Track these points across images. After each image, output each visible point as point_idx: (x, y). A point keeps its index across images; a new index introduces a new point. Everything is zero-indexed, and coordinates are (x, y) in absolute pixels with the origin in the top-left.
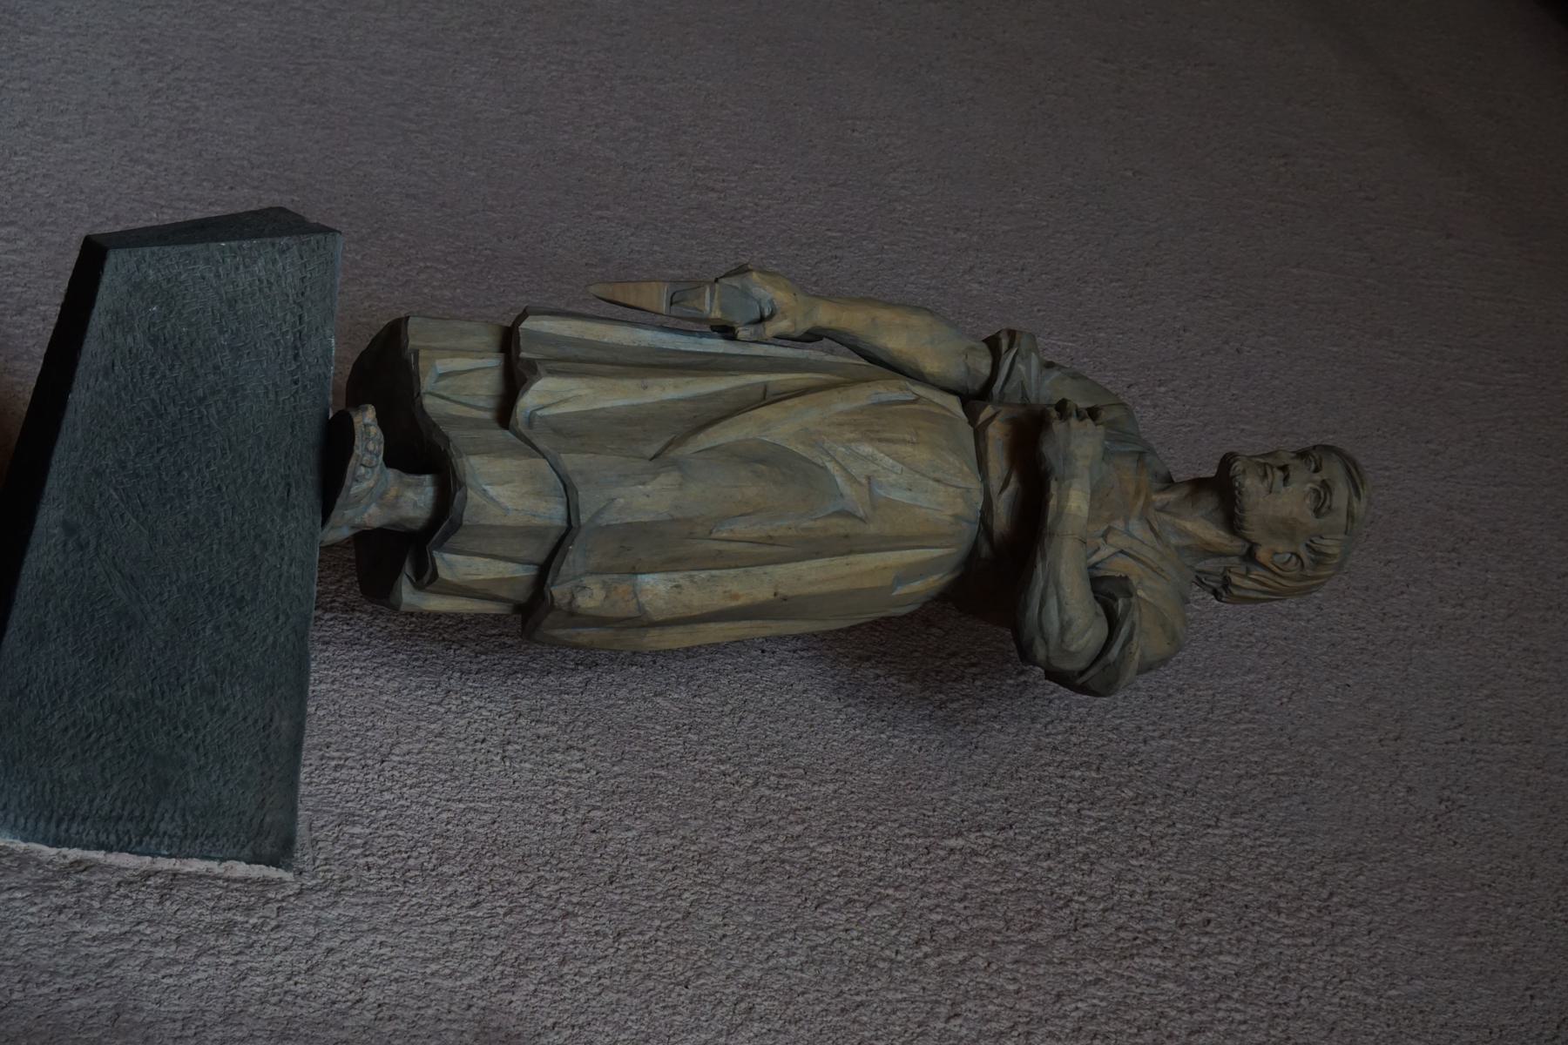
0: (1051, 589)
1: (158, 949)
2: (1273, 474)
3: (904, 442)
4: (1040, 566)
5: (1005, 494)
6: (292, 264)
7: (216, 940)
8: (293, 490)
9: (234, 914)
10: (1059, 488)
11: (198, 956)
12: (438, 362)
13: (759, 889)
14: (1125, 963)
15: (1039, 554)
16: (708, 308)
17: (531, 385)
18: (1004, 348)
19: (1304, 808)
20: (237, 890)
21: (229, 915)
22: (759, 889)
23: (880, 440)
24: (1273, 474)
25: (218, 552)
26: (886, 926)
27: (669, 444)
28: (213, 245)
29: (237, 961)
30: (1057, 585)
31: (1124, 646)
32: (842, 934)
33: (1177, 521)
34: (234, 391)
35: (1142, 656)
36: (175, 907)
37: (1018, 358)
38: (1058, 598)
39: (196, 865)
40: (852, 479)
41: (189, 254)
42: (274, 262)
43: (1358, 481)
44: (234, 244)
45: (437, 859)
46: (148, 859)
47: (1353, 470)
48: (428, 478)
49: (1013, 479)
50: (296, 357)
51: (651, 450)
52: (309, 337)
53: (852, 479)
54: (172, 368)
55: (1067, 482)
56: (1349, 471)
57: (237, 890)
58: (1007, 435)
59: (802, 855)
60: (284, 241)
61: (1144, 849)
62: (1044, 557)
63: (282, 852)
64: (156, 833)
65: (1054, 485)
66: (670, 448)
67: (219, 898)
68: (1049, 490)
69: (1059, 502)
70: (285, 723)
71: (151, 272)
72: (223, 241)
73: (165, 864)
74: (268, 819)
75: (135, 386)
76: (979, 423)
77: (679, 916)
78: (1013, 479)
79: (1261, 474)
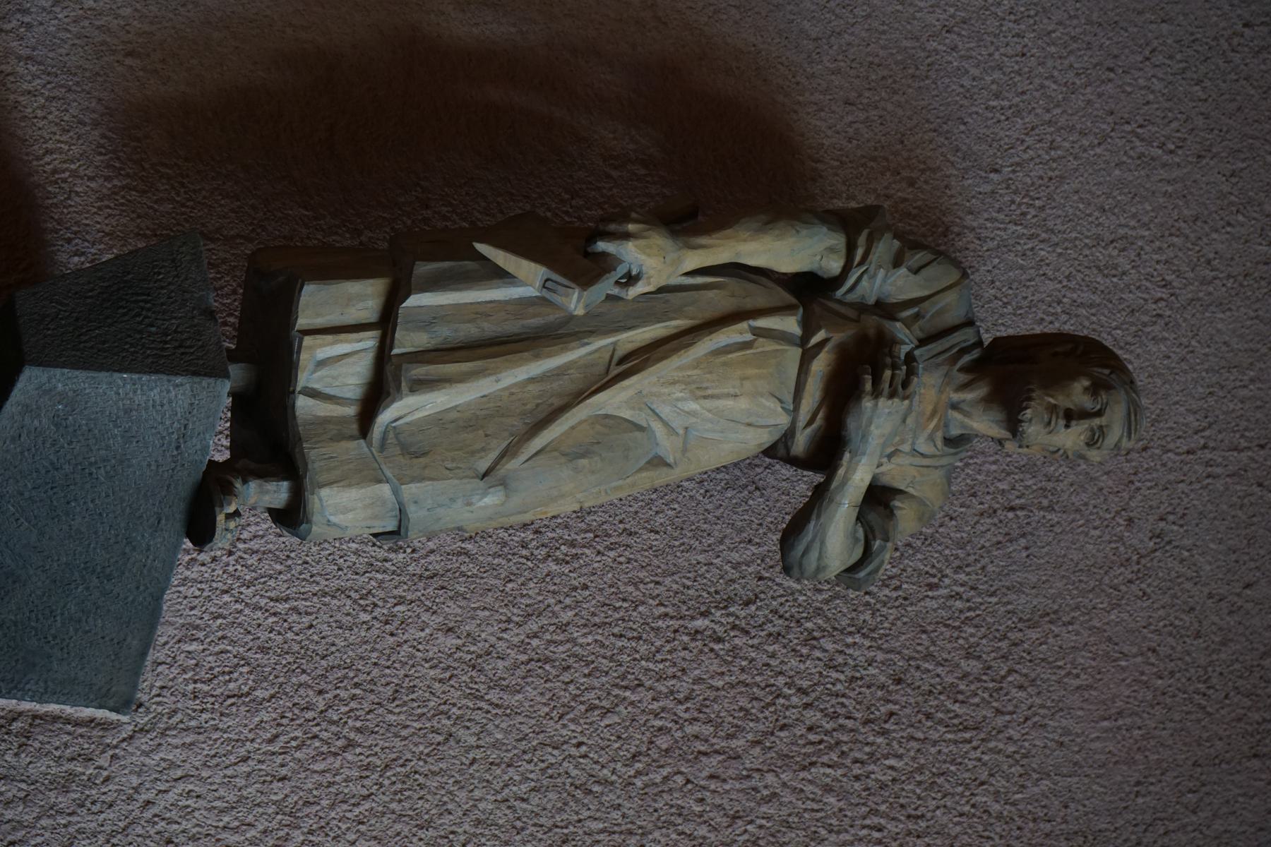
0: (817, 545)
1: (9, 811)
2: (1056, 424)
3: (728, 396)
4: (812, 523)
5: (809, 430)
6: (184, 394)
7: (57, 798)
8: (163, 522)
9: (75, 766)
10: (851, 459)
11: (38, 818)
12: (318, 351)
13: (517, 698)
14: (802, 775)
15: (816, 511)
16: (572, 306)
17: (393, 401)
18: (856, 263)
19: (1024, 554)
20: (82, 736)
21: (71, 766)
22: (517, 698)
23: (705, 397)
24: (1056, 424)
25: (95, 548)
26: (613, 738)
27: (503, 455)
28: (116, 375)
29: (69, 822)
30: (823, 543)
31: (870, 574)
32: (574, 751)
33: (966, 420)
34: (121, 462)
35: (901, 508)
36: (28, 760)
37: (865, 277)
38: (820, 553)
39: (53, 708)
40: (671, 430)
41: (94, 378)
42: (168, 391)
43: (1133, 428)
44: (135, 376)
45: (253, 681)
46: (14, 701)
47: (1133, 418)
48: (285, 485)
49: (820, 415)
50: (178, 448)
51: (483, 465)
52: (192, 438)
53: (671, 430)
54: (70, 443)
55: (858, 458)
56: (1129, 414)
57: (82, 736)
58: (829, 365)
59: (564, 650)
60: (179, 380)
61: (864, 621)
62: (818, 517)
63: (126, 704)
64: (23, 689)
65: (847, 456)
66: (505, 459)
67: (66, 745)
68: (841, 459)
69: (846, 472)
70: (135, 642)
71: (60, 385)
72: (125, 373)
73: (26, 706)
74: (114, 689)
75: (36, 450)
76: (810, 345)
77: (440, 738)
78: (820, 415)
79: (1046, 419)
